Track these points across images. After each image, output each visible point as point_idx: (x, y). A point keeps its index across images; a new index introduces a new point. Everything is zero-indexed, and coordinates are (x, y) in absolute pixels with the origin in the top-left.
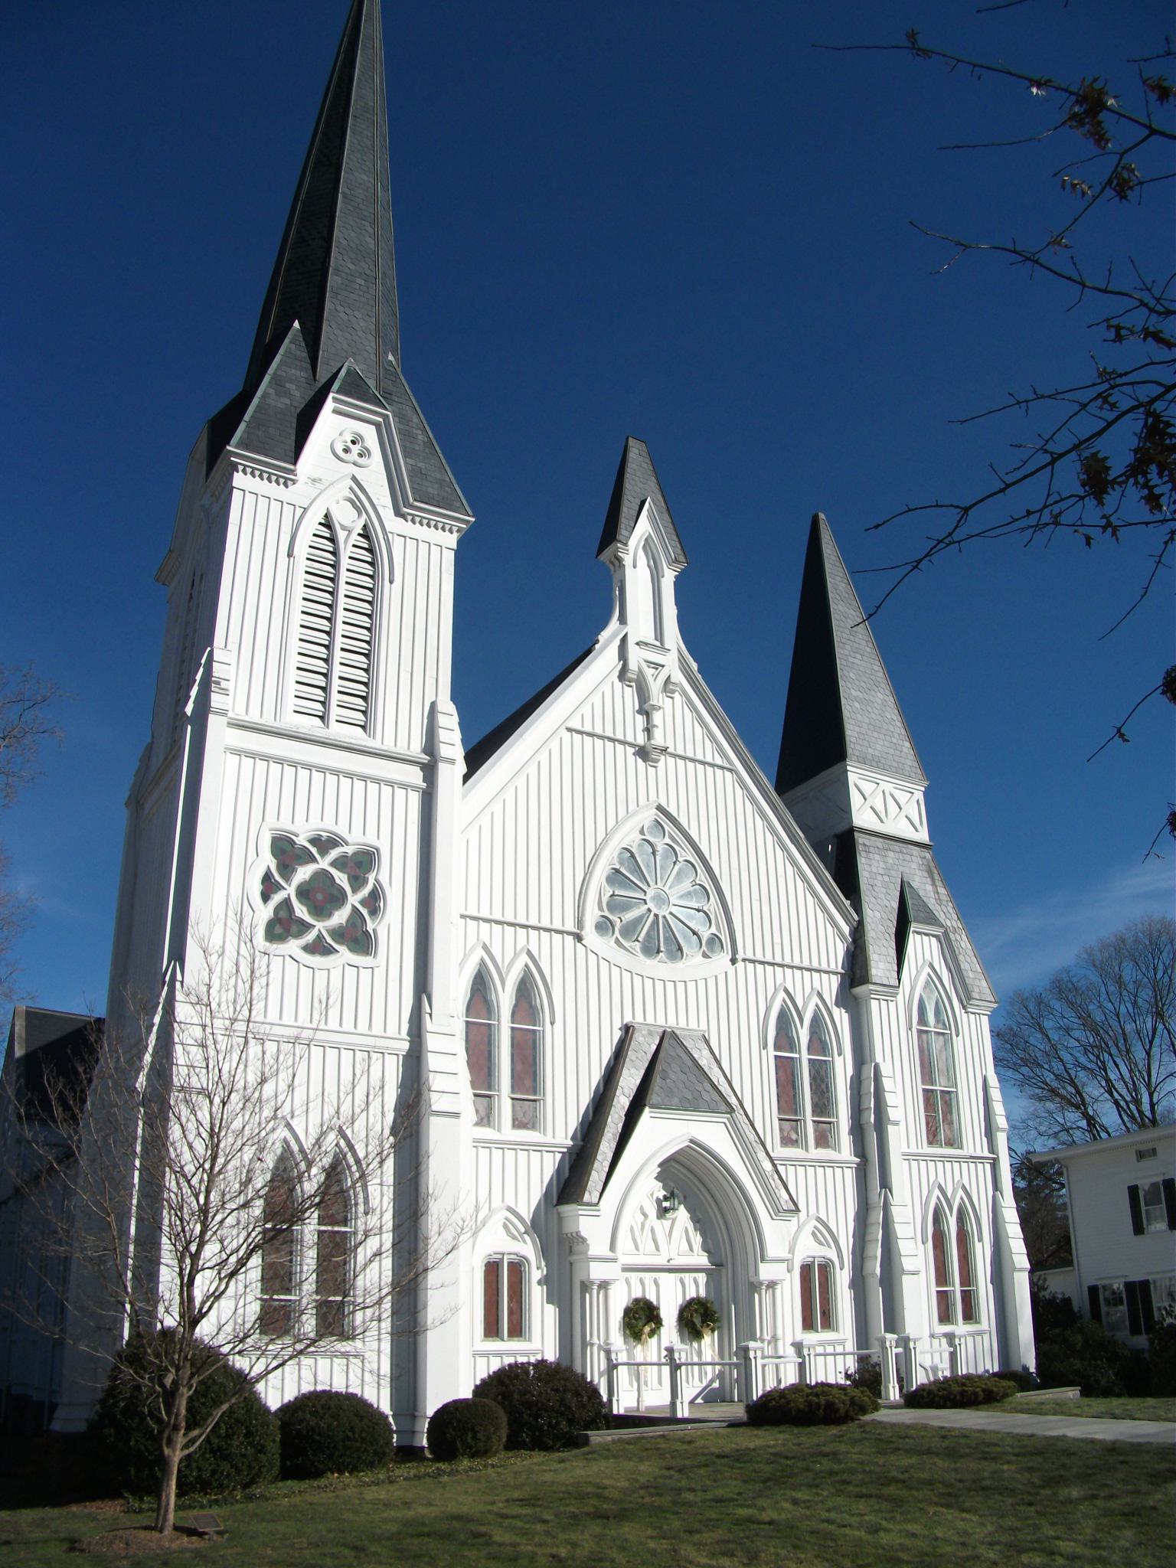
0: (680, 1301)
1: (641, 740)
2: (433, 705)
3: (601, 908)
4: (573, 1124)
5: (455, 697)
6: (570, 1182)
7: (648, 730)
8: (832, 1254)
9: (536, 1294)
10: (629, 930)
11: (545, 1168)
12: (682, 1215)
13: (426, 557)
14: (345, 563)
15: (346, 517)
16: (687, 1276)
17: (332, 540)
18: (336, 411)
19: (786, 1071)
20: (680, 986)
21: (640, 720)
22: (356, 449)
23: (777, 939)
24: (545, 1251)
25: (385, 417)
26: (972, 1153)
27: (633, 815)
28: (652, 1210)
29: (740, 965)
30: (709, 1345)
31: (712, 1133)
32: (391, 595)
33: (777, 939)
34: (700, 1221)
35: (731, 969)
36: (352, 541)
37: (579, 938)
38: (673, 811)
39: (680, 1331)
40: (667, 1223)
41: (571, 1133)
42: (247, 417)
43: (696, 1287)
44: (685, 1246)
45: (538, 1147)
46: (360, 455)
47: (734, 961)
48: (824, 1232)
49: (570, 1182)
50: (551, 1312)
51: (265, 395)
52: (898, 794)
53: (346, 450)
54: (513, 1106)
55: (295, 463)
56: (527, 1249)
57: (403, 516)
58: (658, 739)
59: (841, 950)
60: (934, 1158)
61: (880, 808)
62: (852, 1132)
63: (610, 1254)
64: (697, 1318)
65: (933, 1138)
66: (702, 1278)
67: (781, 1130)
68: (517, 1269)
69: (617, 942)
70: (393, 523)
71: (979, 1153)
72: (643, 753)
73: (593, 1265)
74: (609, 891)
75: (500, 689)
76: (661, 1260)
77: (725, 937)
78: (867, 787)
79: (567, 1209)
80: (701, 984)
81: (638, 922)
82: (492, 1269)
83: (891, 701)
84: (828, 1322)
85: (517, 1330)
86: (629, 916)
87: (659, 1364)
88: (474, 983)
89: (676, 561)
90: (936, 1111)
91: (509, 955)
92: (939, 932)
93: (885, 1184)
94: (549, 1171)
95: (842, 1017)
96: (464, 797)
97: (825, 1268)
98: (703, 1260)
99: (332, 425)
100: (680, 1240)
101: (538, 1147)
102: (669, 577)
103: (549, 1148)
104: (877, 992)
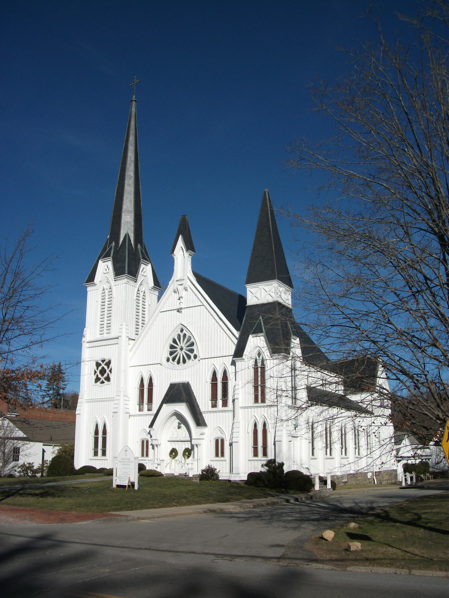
8: (223, 437)
19: (214, 386)
58: (182, 306)
72: (179, 310)
78: (253, 290)
97: (222, 441)
101: (228, 411)
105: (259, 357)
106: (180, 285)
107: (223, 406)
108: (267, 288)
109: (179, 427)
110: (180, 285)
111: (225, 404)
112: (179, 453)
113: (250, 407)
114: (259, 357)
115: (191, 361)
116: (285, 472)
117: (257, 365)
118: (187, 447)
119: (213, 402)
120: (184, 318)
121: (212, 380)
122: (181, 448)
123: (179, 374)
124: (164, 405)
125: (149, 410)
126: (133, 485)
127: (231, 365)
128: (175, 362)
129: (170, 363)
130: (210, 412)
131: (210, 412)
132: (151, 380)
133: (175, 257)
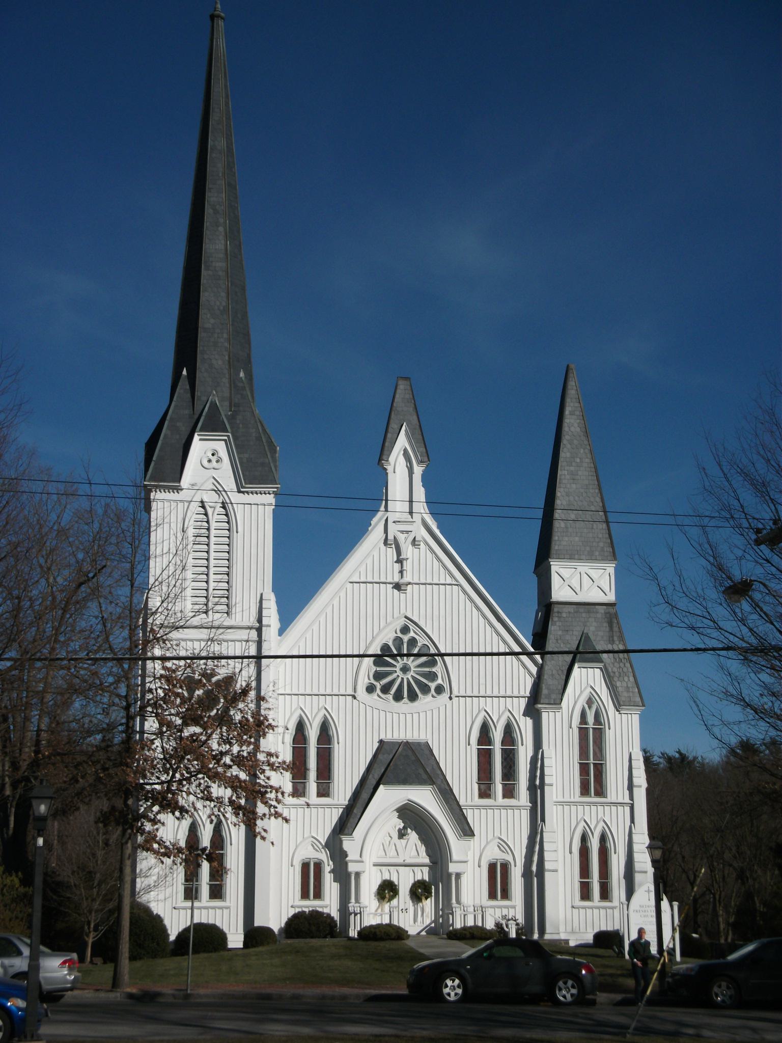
0: (412, 882)
1: (397, 579)
2: (262, 595)
3: (369, 679)
4: (349, 795)
5: (274, 590)
6: (347, 822)
7: (401, 572)
8: (510, 859)
9: (328, 878)
10: (385, 689)
11: (334, 816)
12: (413, 836)
13: (257, 512)
14: (213, 525)
15: (210, 498)
16: (416, 869)
17: (206, 514)
18: (201, 440)
19: (485, 758)
20: (416, 716)
21: (397, 567)
22: (214, 459)
23: (482, 681)
24: (332, 858)
25: (228, 436)
26: (614, 800)
27: (390, 624)
28: (395, 835)
29: (455, 700)
30: (428, 904)
31: (424, 797)
32: (238, 539)
33: (482, 681)
34: (424, 839)
35: (449, 703)
36: (216, 512)
37: (354, 697)
38: (415, 619)
39: (412, 898)
40: (403, 842)
41: (348, 798)
42: (154, 458)
43: (423, 874)
44: (414, 853)
45: (329, 806)
46: (217, 461)
47: (450, 698)
48: (503, 845)
49: (347, 822)
50: (336, 887)
51: (165, 435)
52: (593, 573)
53: (210, 461)
54: (318, 786)
55: (179, 481)
56: (323, 856)
57: (243, 492)
58: (407, 578)
59: (529, 682)
60: (582, 804)
61: (576, 585)
62: (529, 789)
63: (359, 859)
64: (419, 891)
65: (585, 790)
66: (426, 870)
67: (479, 789)
68: (318, 866)
69: (378, 696)
70: (235, 497)
71: (620, 800)
72: (397, 586)
73: (350, 864)
74: (374, 669)
75: (301, 571)
76: (400, 861)
77: (447, 686)
78: (565, 573)
79: (344, 838)
80: (429, 713)
81: (391, 683)
82: (305, 866)
83: (553, 543)
84: (506, 895)
85: (318, 895)
86: (384, 681)
87: (192, 908)
88: (190, 827)
89: (421, 462)
90: (588, 774)
91: (315, 711)
92: (601, 665)
93: (543, 820)
94: (335, 819)
95: (525, 726)
96: (280, 641)
97: (505, 867)
98: (427, 860)
99: (200, 447)
100: (413, 848)
101: (329, 806)
102: (418, 470)
103: (336, 806)
104: (545, 708)
105: (590, 707)
106: (402, 532)
107: (504, 796)
108: (594, 573)
109: (402, 834)
110: (402, 532)
111: (509, 792)
112: (407, 892)
113: (569, 803)
114: (590, 707)
115: (429, 698)
116: (172, 938)
117: (586, 723)
118: (419, 877)
119: (482, 787)
120: (413, 604)
121: (295, 741)
122: (405, 881)
123: (407, 723)
124: (381, 787)
125: (323, 792)
126: (70, 962)
127: (524, 715)
128: (390, 697)
129: (376, 697)
130: (479, 807)
131: (479, 807)
132: (325, 729)
133: (390, 469)
